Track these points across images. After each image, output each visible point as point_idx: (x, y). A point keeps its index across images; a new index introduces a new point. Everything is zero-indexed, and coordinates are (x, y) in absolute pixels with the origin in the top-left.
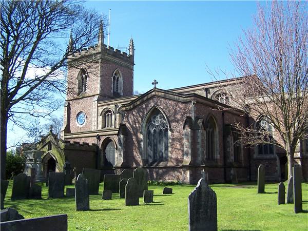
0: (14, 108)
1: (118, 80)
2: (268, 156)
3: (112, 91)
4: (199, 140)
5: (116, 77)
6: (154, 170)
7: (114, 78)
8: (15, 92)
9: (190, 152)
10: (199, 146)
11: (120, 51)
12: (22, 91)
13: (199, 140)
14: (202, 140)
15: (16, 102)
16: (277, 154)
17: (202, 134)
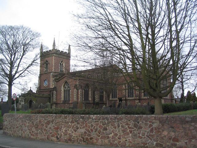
0: (14, 82)
1: (62, 65)
2: (115, 99)
3: (59, 70)
4: (80, 93)
5: (62, 63)
6: (127, 98)
7: (61, 64)
8: (14, 76)
9: (6, 114)
10: (79, 95)
11: (63, 52)
12: (17, 75)
13: (80, 93)
14: (81, 93)
15: (16, 78)
16: (118, 98)
17: (81, 91)
